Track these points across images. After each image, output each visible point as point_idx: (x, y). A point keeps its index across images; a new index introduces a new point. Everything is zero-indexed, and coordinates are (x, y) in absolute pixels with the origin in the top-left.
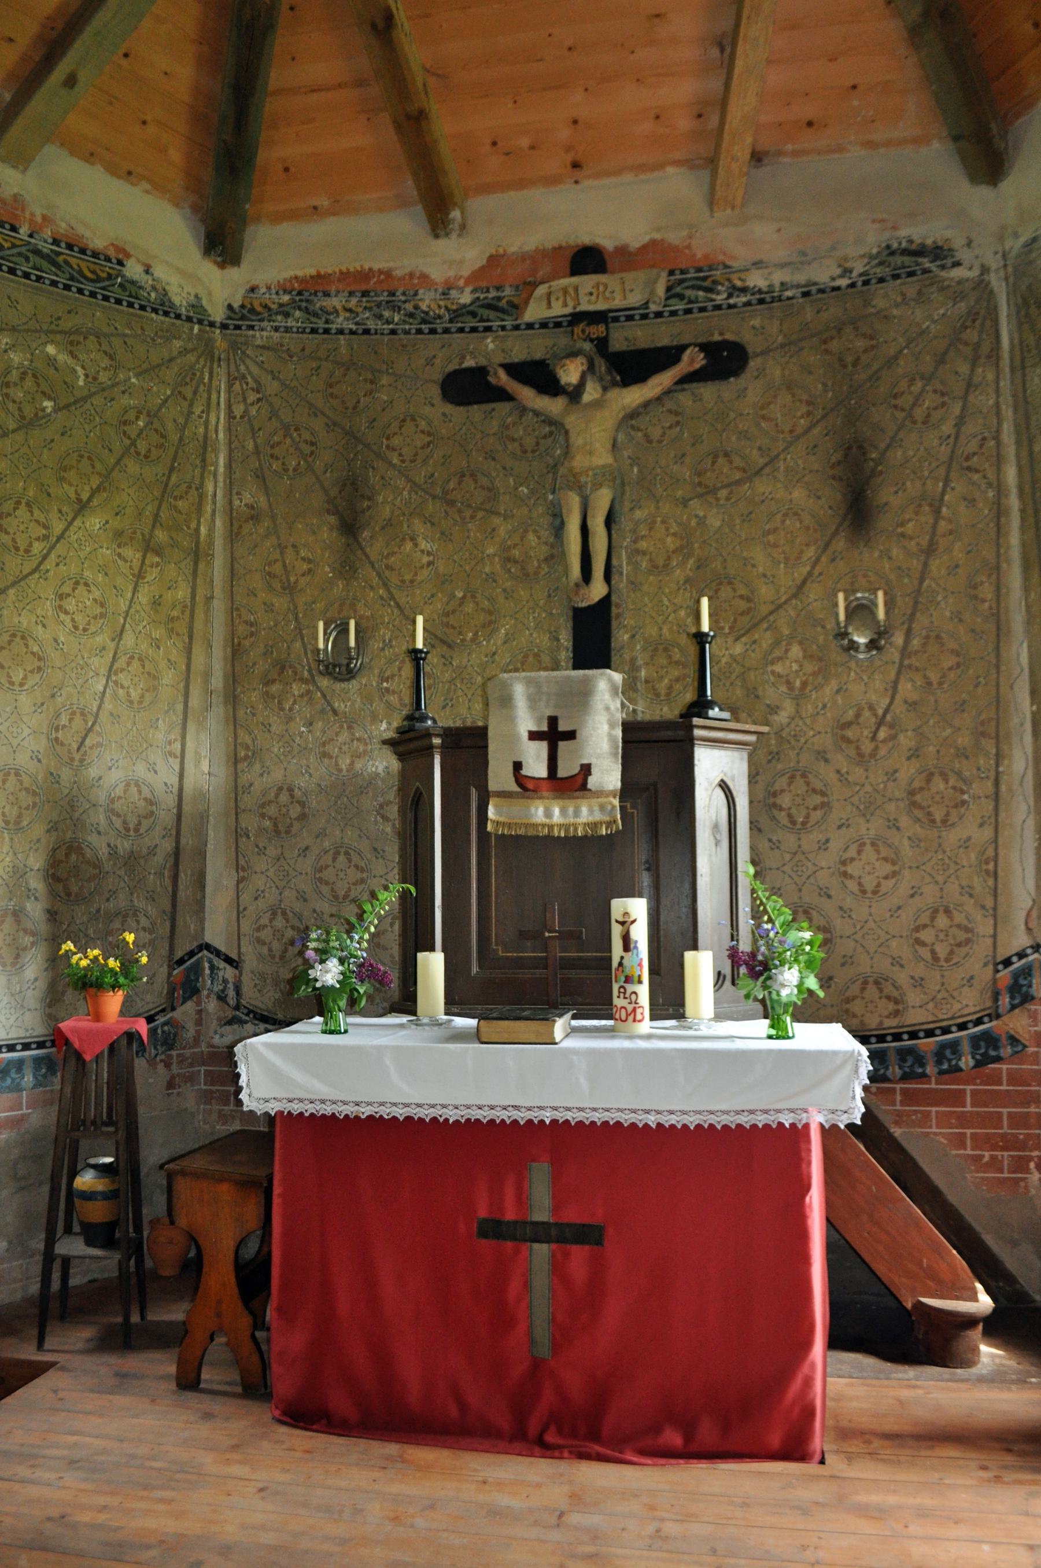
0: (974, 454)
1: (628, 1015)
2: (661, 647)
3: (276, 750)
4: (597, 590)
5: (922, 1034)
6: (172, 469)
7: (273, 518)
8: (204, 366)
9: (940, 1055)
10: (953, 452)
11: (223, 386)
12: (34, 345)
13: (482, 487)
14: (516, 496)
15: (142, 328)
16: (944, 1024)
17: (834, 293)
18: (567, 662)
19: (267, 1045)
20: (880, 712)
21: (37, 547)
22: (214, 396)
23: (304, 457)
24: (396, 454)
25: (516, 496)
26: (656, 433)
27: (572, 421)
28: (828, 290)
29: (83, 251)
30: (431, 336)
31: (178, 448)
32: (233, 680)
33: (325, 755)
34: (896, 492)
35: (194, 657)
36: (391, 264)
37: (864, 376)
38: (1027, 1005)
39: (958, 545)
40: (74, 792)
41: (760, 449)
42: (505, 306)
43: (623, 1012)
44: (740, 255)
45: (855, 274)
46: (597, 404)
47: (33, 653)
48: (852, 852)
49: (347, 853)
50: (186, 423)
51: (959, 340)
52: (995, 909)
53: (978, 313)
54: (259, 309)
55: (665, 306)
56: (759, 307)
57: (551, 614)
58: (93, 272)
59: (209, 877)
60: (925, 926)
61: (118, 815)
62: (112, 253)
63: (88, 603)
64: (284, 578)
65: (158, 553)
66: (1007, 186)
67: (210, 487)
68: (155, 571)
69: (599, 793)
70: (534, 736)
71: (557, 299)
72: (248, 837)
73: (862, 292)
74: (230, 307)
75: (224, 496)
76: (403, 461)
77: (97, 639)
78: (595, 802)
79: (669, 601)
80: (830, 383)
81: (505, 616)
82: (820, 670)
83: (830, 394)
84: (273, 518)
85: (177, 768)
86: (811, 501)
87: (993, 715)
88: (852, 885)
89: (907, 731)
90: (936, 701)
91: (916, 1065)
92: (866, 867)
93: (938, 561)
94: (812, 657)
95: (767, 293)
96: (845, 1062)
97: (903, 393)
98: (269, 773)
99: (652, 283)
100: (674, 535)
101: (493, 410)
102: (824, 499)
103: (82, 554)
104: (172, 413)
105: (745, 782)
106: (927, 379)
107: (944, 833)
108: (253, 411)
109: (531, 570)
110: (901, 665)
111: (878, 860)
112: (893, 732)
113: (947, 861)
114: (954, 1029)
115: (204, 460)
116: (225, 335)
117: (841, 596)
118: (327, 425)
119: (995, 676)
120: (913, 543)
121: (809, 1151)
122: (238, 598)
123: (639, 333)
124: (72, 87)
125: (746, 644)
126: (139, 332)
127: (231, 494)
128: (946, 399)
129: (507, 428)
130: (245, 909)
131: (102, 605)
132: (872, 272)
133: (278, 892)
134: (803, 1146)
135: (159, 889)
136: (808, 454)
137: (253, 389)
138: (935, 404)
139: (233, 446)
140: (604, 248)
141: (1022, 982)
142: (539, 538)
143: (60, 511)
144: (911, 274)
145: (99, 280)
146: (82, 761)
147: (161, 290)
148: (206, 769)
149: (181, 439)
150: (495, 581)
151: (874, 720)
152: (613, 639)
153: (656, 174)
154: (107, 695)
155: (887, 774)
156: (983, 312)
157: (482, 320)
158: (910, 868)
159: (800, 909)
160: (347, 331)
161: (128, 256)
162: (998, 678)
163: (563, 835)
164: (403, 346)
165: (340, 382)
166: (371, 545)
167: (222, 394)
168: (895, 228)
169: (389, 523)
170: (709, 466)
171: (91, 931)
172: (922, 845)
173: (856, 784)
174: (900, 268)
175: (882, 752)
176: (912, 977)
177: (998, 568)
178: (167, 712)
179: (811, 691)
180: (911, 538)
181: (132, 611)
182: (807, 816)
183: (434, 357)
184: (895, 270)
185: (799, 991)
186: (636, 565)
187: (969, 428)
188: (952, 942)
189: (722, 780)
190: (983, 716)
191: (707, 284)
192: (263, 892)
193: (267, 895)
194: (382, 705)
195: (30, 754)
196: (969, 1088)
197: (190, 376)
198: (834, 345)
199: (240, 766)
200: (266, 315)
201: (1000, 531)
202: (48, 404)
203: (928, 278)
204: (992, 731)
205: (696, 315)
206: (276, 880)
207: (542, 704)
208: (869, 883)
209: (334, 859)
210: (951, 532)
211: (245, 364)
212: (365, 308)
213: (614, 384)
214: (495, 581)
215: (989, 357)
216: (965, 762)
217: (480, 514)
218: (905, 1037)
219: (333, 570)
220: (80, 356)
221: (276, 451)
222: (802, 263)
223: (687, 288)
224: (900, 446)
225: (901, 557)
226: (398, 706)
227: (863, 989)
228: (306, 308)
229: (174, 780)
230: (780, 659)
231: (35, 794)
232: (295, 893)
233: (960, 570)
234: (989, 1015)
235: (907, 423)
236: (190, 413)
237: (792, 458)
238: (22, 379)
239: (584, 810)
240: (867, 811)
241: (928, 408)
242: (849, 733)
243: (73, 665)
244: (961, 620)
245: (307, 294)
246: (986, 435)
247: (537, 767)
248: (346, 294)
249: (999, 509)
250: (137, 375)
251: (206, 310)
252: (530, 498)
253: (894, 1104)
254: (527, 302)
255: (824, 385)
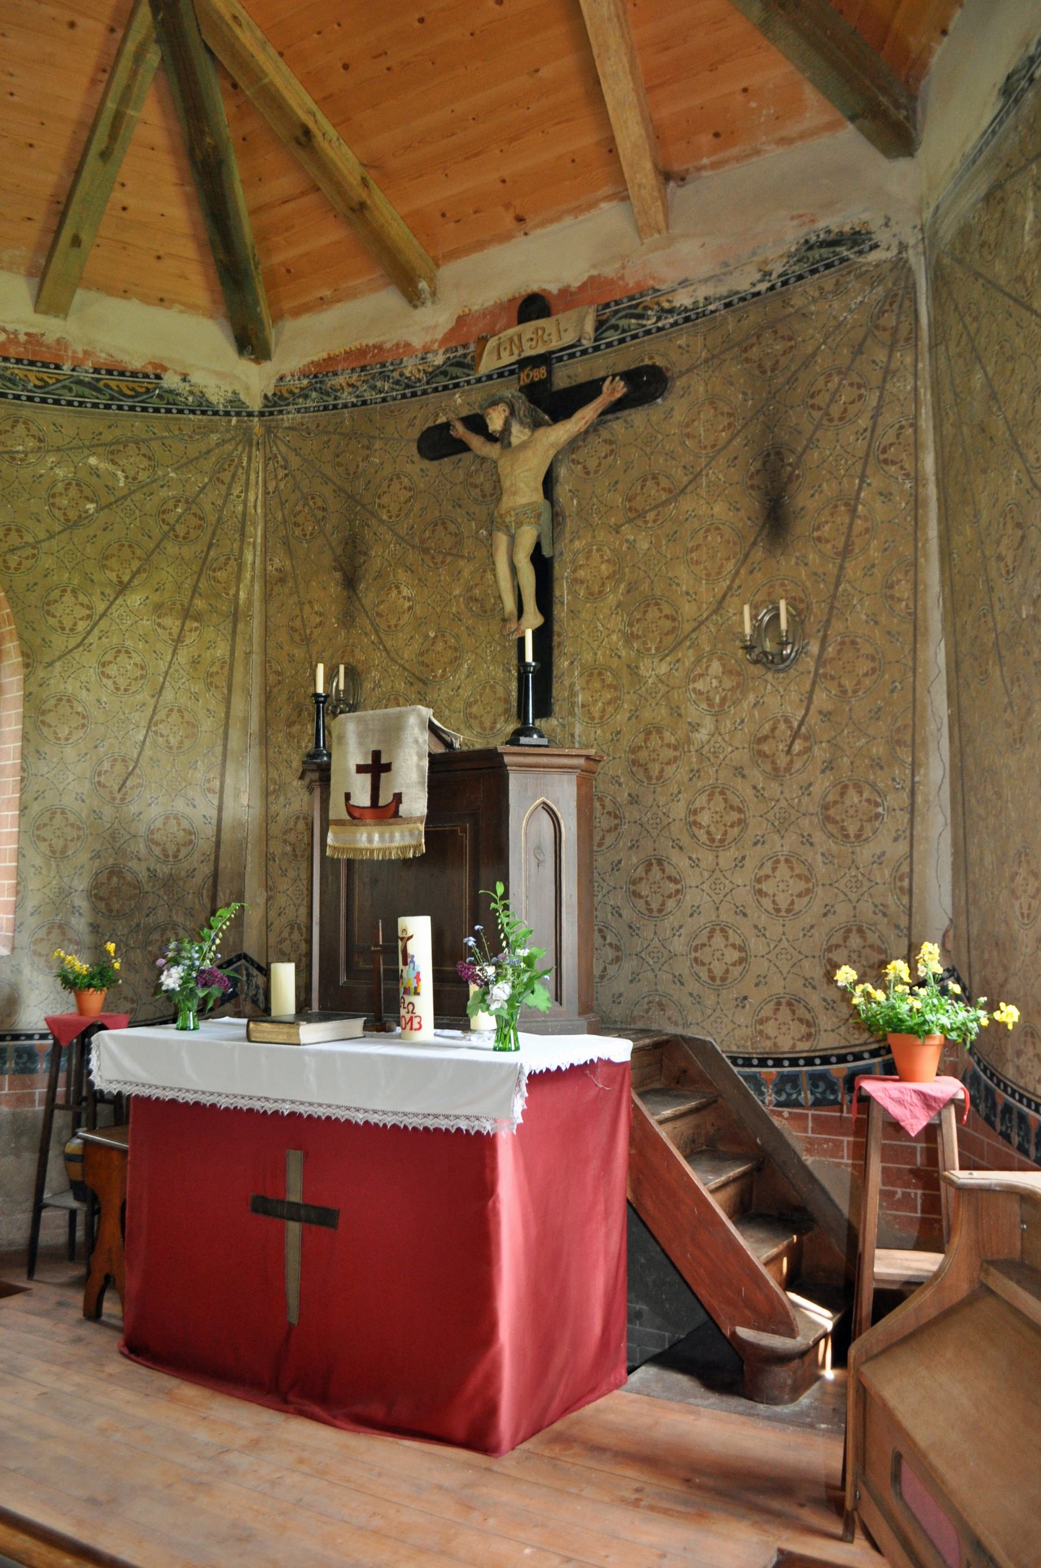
0: (891, 445)
1: (406, 1024)
2: (596, 672)
5: (834, 1059)
6: (210, 546)
8: (243, 452)
10: (869, 446)
12: (76, 460)
14: (477, 538)
15: (180, 429)
16: (857, 1049)
17: (755, 299)
19: (112, 1037)
20: (795, 724)
21: (82, 626)
22: (253, 476)
23: (318, 522)
24: (385, 511)
25: (477, 538)
26: (592, 464)
28: (748, 297)
29: (122, 374)
30: (413, 399)
31: (216, 526)
32: (266, 723)
34: (812, 495)
35: (233, 707)
36: (382, 338)
37: (782, 380)
39: (875, 543)
40: (116, 826)
41: (685, 467)
45: (774, 275)
46: (524, 446)
47: (78, 713)
48: (767, 870)
50: (224, 505)
51: (877, 327)
52: (909, 929)
54: (286, 395)
57: (504, 647)
58: (133, 389)
60: (838, 946)
61: (157, 844)
62: (150, 370)
63: (129, 668)
66: (920, 153)
67: (249, 557)
69: (410, 820)
70: (361, 769)
72: (274, 861)
74: (266, 397)
75: (261, 563)
77: (138, 697)
79: (603, 626)
80: (750, 392)
82: (738, 684)
83: (750, 402)
85: (216, 802)
88: (767, 902)
89: (821, 742)
90: (850, 709)
91: (828, 1092)
92: (780, 884)
93: (854, 562)
94: (731, 672)
95: (693, 310)
97: (820, 391)
99: (581, 321)
100: (608, 561)
101: (460, 460)
102: (743, 511)
103: (123, 627)
106: (843, 373)
108: (282, 485)
109: (488, 607)
111: (791, 877)
112: (807, 744)
113: (860, 877)
114: (866, 1055)
115: (243, 534)
118: (334, 491)
119: (911, 680)
120: (829, 546)
122: (269, 651)
124: (79, 245)
126: (177, 432)
128: (863, 391)
129: (471, 476)
131: (142, 668)
137: (281, 466)
138: (851, 399)
143: (103, 594)
144: (828, 266)
145: (138, 394)
146: (123, 799)
147: (198, 393)
148: (245, 803)
149: (219, 519)
150: (460, 620)
152: (554, 668)
153: (593, 212)
154: (147, 743)
155: (801, 788)
158: (823, 885)
159: (718, 928)
161: (165, 369)
162: (914, 682)
164: (392, 412)
169: (379, 575)
171: (131, 942)
172: (836, 861)
174: (818, 262)
175: (797, 765)
176: (825, 1000)
177: (915, 564)
178: (205, 755)
179: (729, 707)
180: (827, 541)
181: (172, 670)
182: (725, 833)
183: (415, 417)
184: (813, 264)
187: (888, 418)
188: (865, 963)
191: (639, 310)
195: (74, 796)
197: (228, 463)
198: (755, 352)
199: (271, 798)
202: (91, 507)
204: (908, 739)
205: (629, 343)
206: (294, 898)
208: (783, 901)
210: (867, 530)
211: (276, 445)
212: (364, 382)
214: (460, 620)
215: (907, 340)
216: (879, 772)
217: (449, 559)
219: (338, 621)
220: (120, 462)
222: (725, 274)
223: (621, 318)
228: (321, 388)
229: (214, 813)
230: (701, 675)
231: (79, 828)
235: (825, 422)
237: (714, 473)
238: (66, 489)
239: (397, 835)
240: (781, 827)
241: (844, 403)
242: (766, 748)
243: (115, 720)
244: (876, 623)
245: (320, 376)
246: (903, 423)
247: (362, 798)
248: (349, 371)
249: (916, 500)
250: (175, 470)
253: (806, 1130)
255: (745, 394)
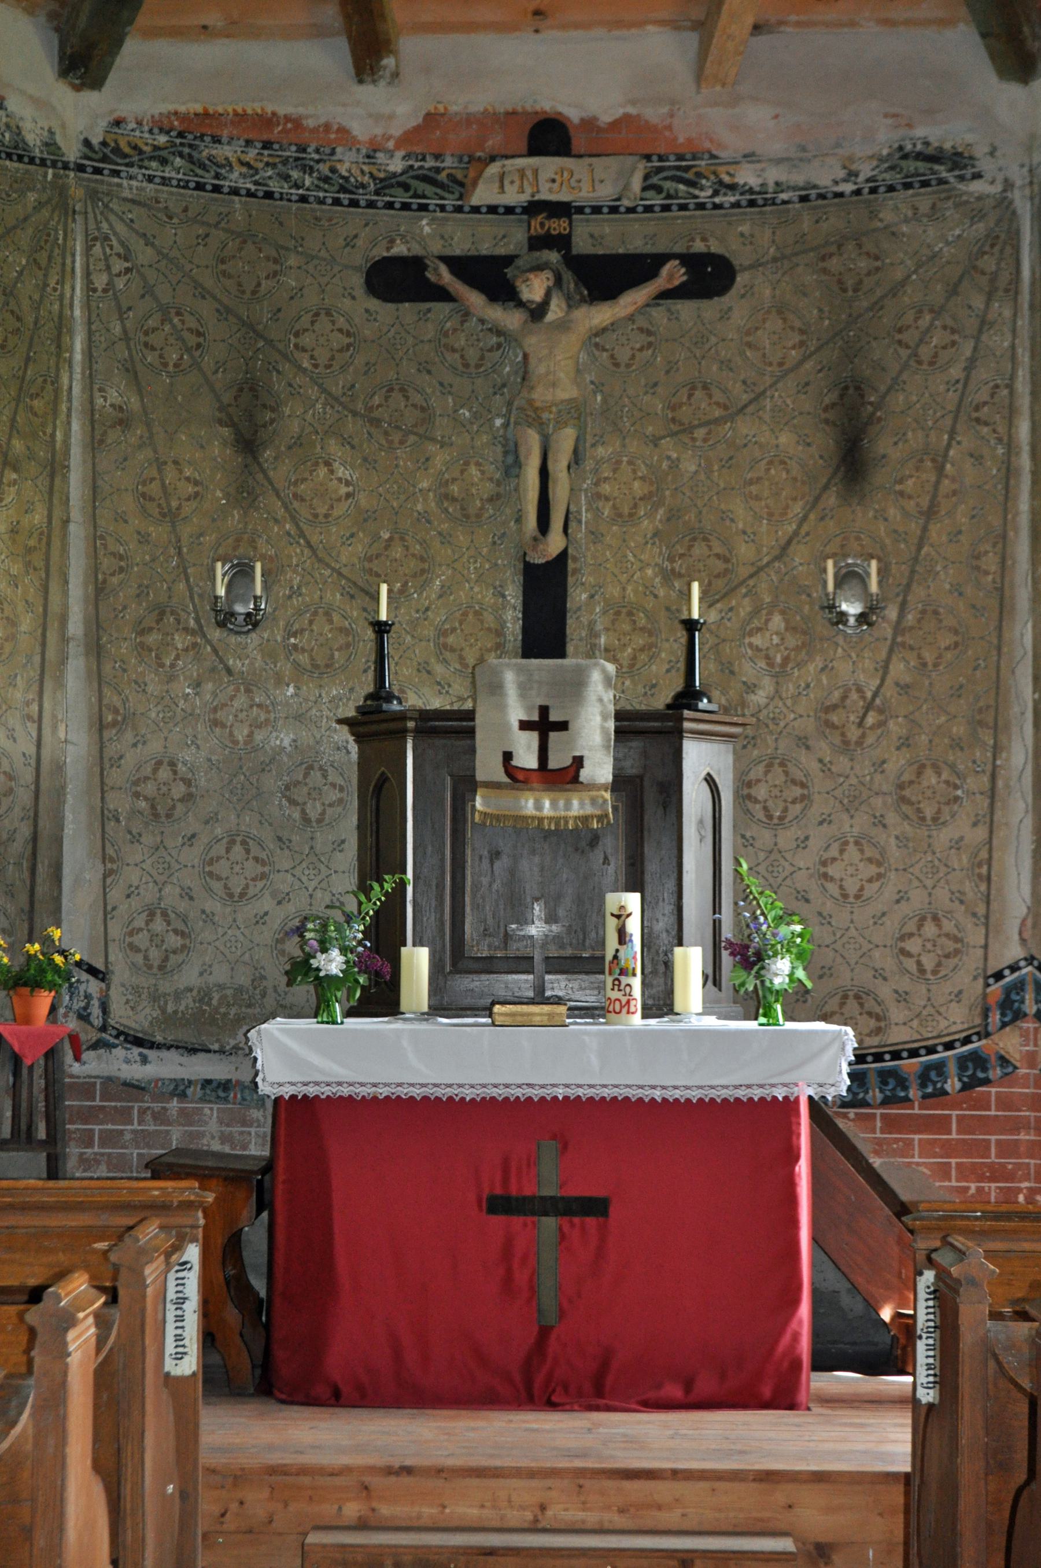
0: (985, 403)
1: (622, 1007)
3: (153, 715)
4: (555, 543)
5: (905, 1054)
7: (148, 425)
9: (924, 1078)
10: (961, 401)
11: (78, 248)
13: (414, 406)
17: (836, 200)
18: (514, 624)
20: (869, 695)
22: (68, 261)
23: (188, 350)
26: (623, 355)
27: (533, 342)
28: (829, 195)
33: (216, 723)
34: (896, 443)
36: (301, 110)
37: (865, 304)
38: (1018, 1023)
41: (744, 382)
42: (446, 181)
43: (617, 1004)
44: (731, 145)
45: (861, 178)
46: (563, 326)
48: (834, 852)
49: (244, 843)
51: (975, 268)
52: (987, 917)
53: (997, 237)
54: (127, 150)
55: (642, 199)
56: (748, 210)
57: (496, 565)
59: (66, 870)
64: (162, 501)
65: (15, 470)
68: (13, 490)
69: (592, 786)
70: (525, 725)
71: (512, 182)
72: (118, 821)
73: (870, 201)
75: (83, 390)
76: (316, 366)
78: (586, 795)
79: (635, 556)
81: (440, 565)
82: (804, 645)
83: (827, 322)
84: (148, 425)
85: (34, 734)
86: (800, 448)
87: (992, 703)
88: (833, 889)
95: (759, 193)
96: (834, 1040)
97: (909, 327)
98: (144, 743)
101: (429, 310)
104: (27, 288)
105: (730, 776)
106: (937, 312)
107: (935, 833)
108: (120, 283)
109: (472, 511)
110: (894, 639)
112: (882, 718)
113: (936, 863)
114: (940, 1048)
115: (59, 347)
116: (80, 179)
117: (830, 563)
118: (218, 311)
119: (995, 658)
120: (912, 503)
121: (799, 1124)
122: (101, 522)
123: (607, 230)
125: (721, 611)
127: (91, 389)
129: (446, 335)
130: (114, 909)
132: (880, 178)
133: (156, 889)
134: (794, 1120)
135: (18, 882)
136: (799, 392)
137: (119, 255)
139: (93, 327)
140: (568, 119)
141: (1014, 997)
142: (483, 472)
144: (925, 184)
147: (14, 129)
150: (429, 522)
151: (861, 703)
153: (634, 31)
156: (1003, 236)
157: (416, 196)
158: (896, 870)
160: (243, 192)
162: (998, 661)
163: (553, 828)
165: (234, 257)
166: (275, 469)
167: (78, 258)
168: (909, 126)
169: (298, 442)
170: (684, 400)
172: (911, 845)
173: (840, 775)
174: (912, 176)
175: (870, 740)
176: (896, 992)
177: (1004, 536)
178: (25, 666)
180: (910, 497)
182: (785, 810)
183: (356, 236)
184: (907, 177)
185: (791, 981)
186: (597, 513)
187: (982, 373)
188: (940, 952)
189: (709, 774)
190: (981, 704)
191: (689, 175)
192: (137, 888)
193: (142, 891)
194: (289, 665)
196: (955, 1113)
198: (834, 264)
199: (106, 734)
200: (136, 158)
201: (1008, 495)
203: (944, 191)
204: (990, 720)
205: (675, 213)
206: (154, 873)
207: (534, 692)
209: (228, 850)
210: (954, 493)
211: (107, 220)
212: (267, 164)
213: (583, 300)
214: (429, 522)
215: (1007, 291)
216: (959, 754)
217: (412, 438)
218: (887, 1057)
219: (227, 496)
221: (152, 339)
222: (801, 160)
223: (666, 179)
224: (903, 390)
225: (899, 518)
226: (309, 667)
227: (842, 1004)
229: (32, 750)
232: (178, 890)
233: (962, 538)
234: (978, 1033)
235: (912, 363)
236: (46, 285)
237: (780, 397)
239: (575, 803)
240: (851, 804)
242: (834, 718)
244: (960, 594)
247: (527, 758)
248: (242, 143)
249: (1008, 469)
251: (59, 148)
252: (472, 423)
254: (475, 183)
255: (821, 310)
